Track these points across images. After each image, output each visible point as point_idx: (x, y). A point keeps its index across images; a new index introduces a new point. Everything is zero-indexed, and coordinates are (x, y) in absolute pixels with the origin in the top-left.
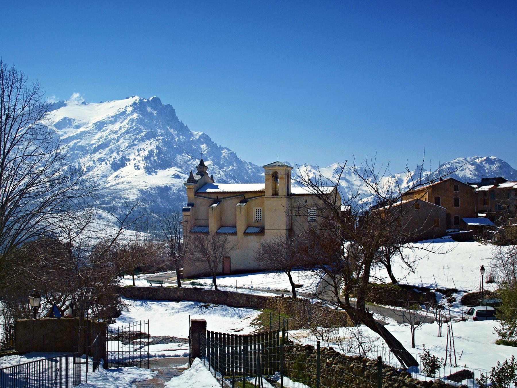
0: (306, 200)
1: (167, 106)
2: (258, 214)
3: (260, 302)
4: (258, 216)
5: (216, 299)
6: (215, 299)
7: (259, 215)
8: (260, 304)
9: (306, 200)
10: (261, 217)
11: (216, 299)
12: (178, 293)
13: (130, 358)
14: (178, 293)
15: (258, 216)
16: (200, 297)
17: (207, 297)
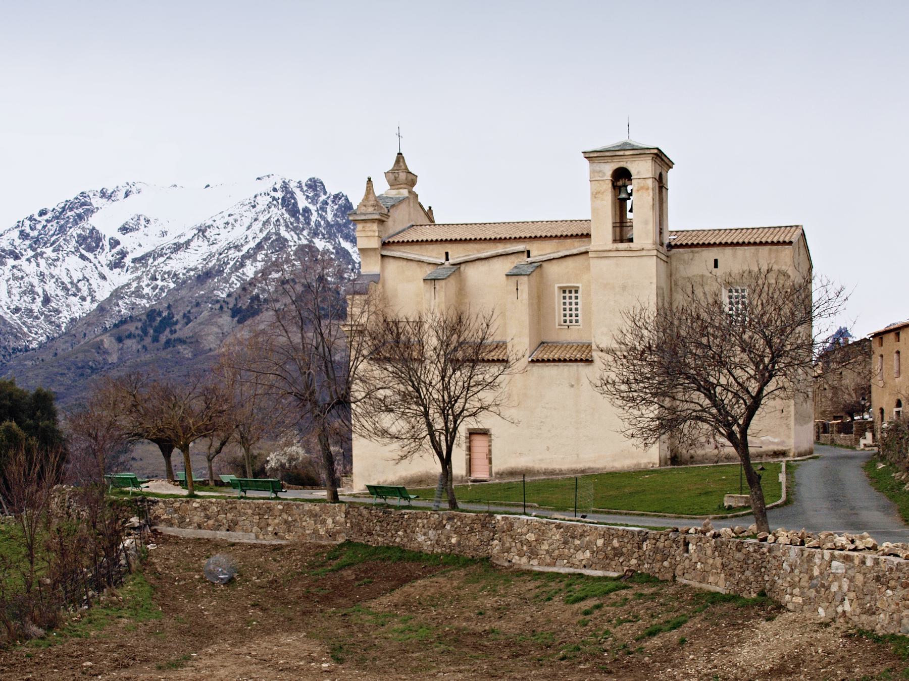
0: (716, 261)
1: (337, 197)
2: (571, 309)
3: (614, 549)
4: (570, 304)
5: (454, 541)
6: (448, 538)
7: (574, 312)
8: (615, 555)
9: (716, 261)
10: (579, 312)
11: (454, 541)
12: (329, 521)
13: (732, 417)
14: (329, 521)
15: (570, 304)
16: (400, 533)
17: (425, 534)
